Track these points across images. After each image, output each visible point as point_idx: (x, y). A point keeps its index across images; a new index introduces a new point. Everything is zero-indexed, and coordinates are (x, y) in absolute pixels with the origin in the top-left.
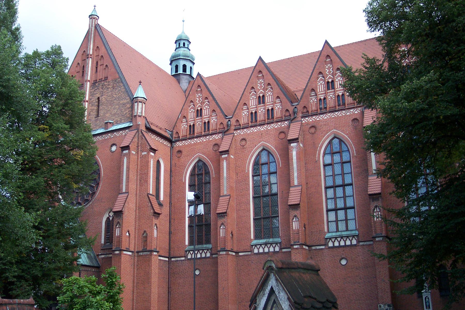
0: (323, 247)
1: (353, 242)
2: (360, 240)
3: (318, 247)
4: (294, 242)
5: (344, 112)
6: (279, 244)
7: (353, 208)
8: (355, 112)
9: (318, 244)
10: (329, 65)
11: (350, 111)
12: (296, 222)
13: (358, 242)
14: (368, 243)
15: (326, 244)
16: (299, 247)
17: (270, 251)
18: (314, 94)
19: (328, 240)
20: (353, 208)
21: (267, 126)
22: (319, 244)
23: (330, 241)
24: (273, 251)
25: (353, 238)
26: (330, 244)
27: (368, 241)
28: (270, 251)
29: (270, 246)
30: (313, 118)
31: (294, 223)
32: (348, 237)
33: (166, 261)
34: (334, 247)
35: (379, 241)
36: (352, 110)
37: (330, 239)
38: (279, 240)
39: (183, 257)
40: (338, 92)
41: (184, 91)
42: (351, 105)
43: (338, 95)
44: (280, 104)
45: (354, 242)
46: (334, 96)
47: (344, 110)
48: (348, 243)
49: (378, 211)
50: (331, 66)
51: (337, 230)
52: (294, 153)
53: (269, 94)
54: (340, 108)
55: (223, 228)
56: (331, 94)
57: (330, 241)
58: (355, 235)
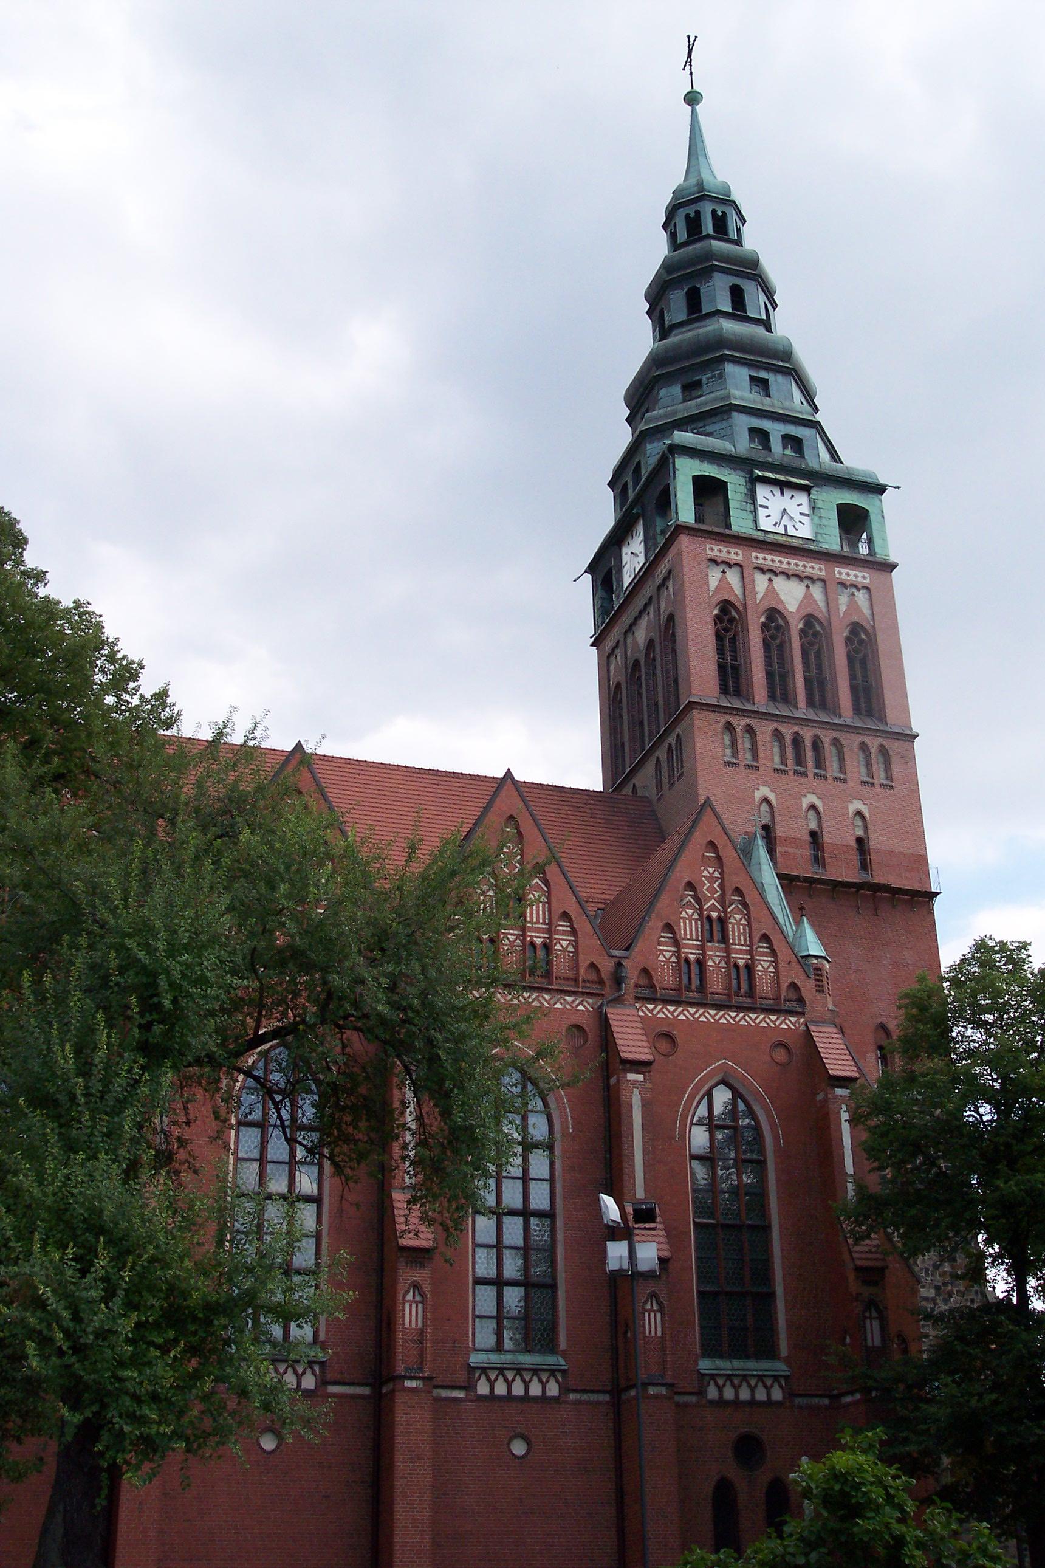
0: (460, 1394)
1: (550, 1390)
2: (329, 1376)
3: (444, 1393)
4: (406, 1369)
5: (547, 997)
6: (317, 1368)
7: (478, 1281)
8: (578, 1006)
9: (444, 1384)
10: (711, 870)
11: (565, 1000)
12: (414, 1305)
13: (564, 1389)
14: (593, 1397)
15: (470, 1387)
16: (421, 1386)
17: (531, 1394)
18: (765, 950)
19: (477, 1375)
20: (478, 1281)
21: (778, 1019)
22: (449, 1384)
23: (483, 1378)
24: (488, 1393)
25: (726, 1381)
26: (483, 1388)
27: (593, 1391)
28: (549, 1394)
29: (287, 1369)
30: (771, 1020)
31: (407, 1305)
32: (536, 1371)
33: (361, 1397)
34: (492, 1397)
35: (656, 1397)
36: (569, 999)
37: (484, 1370)
38: (781, 1368)
39: (460, 1388)
40: (561, 937)
41: (740, 842)
42: (566, 982)
43: (533, 944)
44: (673, 949)
45: (553, 1390)
46: (518, 941)
47: (548, 991)
48: (535, 1390)
49: (655, 1307)
50: (717, 875)
51: (499, 1348)
52: (636, 1100)
53: (690, 914)
54: (539, 982)
55: (413, 1301)
56: (511, 934)
57: (483, 1378)
58: (559, 1367)
